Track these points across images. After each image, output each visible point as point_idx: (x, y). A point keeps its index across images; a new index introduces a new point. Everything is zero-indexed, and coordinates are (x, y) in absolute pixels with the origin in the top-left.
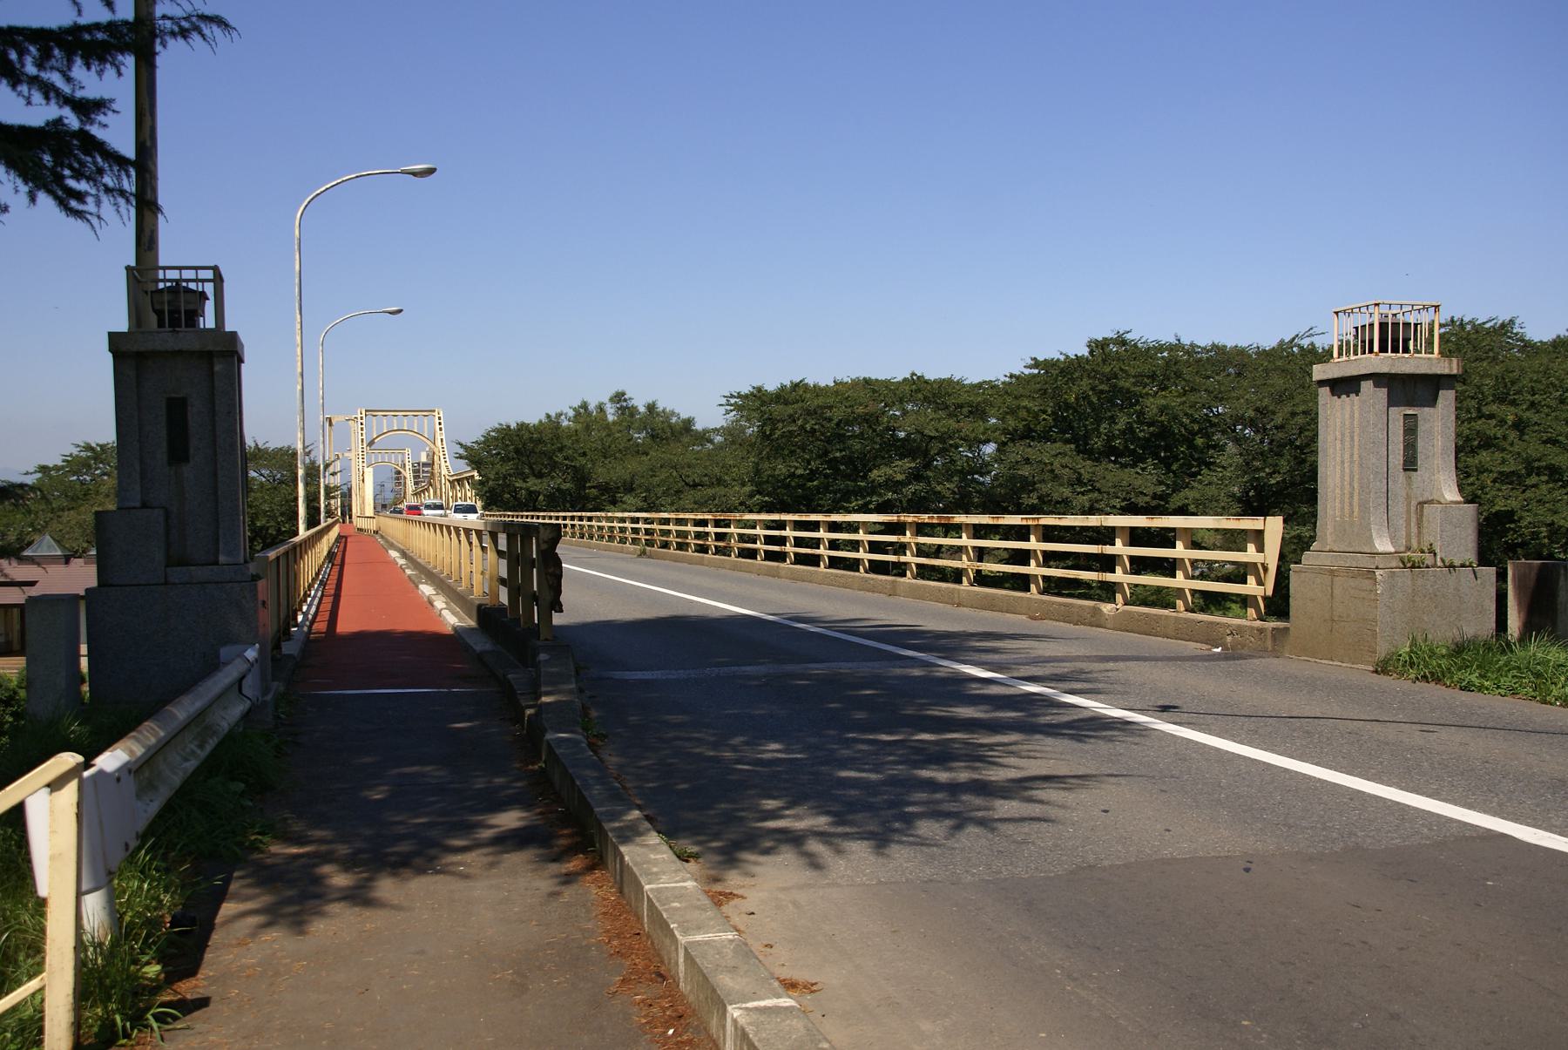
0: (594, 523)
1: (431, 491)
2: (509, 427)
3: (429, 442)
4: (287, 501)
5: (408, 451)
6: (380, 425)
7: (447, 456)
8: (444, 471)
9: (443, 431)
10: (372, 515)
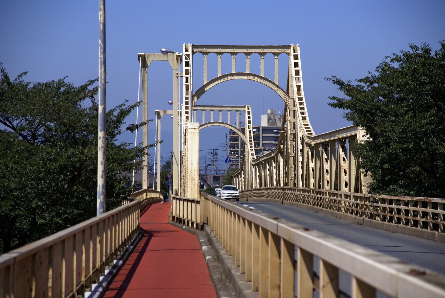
0: (428, 210)
1: (281, 160)
2: (427, 51)
3: (280, 92)
4: (48, 172)
5: (248, 109)
6: (212, 67)
7: (306, 110)
8: (251, 159)
9: (301, 76)
10: (196, 197)
